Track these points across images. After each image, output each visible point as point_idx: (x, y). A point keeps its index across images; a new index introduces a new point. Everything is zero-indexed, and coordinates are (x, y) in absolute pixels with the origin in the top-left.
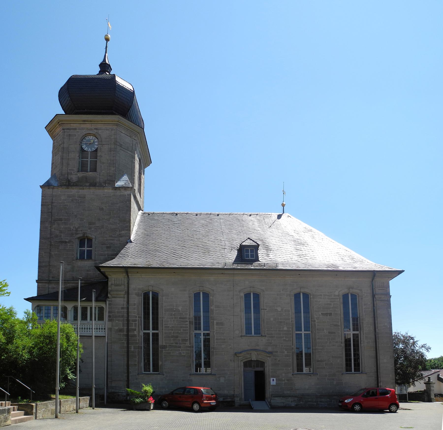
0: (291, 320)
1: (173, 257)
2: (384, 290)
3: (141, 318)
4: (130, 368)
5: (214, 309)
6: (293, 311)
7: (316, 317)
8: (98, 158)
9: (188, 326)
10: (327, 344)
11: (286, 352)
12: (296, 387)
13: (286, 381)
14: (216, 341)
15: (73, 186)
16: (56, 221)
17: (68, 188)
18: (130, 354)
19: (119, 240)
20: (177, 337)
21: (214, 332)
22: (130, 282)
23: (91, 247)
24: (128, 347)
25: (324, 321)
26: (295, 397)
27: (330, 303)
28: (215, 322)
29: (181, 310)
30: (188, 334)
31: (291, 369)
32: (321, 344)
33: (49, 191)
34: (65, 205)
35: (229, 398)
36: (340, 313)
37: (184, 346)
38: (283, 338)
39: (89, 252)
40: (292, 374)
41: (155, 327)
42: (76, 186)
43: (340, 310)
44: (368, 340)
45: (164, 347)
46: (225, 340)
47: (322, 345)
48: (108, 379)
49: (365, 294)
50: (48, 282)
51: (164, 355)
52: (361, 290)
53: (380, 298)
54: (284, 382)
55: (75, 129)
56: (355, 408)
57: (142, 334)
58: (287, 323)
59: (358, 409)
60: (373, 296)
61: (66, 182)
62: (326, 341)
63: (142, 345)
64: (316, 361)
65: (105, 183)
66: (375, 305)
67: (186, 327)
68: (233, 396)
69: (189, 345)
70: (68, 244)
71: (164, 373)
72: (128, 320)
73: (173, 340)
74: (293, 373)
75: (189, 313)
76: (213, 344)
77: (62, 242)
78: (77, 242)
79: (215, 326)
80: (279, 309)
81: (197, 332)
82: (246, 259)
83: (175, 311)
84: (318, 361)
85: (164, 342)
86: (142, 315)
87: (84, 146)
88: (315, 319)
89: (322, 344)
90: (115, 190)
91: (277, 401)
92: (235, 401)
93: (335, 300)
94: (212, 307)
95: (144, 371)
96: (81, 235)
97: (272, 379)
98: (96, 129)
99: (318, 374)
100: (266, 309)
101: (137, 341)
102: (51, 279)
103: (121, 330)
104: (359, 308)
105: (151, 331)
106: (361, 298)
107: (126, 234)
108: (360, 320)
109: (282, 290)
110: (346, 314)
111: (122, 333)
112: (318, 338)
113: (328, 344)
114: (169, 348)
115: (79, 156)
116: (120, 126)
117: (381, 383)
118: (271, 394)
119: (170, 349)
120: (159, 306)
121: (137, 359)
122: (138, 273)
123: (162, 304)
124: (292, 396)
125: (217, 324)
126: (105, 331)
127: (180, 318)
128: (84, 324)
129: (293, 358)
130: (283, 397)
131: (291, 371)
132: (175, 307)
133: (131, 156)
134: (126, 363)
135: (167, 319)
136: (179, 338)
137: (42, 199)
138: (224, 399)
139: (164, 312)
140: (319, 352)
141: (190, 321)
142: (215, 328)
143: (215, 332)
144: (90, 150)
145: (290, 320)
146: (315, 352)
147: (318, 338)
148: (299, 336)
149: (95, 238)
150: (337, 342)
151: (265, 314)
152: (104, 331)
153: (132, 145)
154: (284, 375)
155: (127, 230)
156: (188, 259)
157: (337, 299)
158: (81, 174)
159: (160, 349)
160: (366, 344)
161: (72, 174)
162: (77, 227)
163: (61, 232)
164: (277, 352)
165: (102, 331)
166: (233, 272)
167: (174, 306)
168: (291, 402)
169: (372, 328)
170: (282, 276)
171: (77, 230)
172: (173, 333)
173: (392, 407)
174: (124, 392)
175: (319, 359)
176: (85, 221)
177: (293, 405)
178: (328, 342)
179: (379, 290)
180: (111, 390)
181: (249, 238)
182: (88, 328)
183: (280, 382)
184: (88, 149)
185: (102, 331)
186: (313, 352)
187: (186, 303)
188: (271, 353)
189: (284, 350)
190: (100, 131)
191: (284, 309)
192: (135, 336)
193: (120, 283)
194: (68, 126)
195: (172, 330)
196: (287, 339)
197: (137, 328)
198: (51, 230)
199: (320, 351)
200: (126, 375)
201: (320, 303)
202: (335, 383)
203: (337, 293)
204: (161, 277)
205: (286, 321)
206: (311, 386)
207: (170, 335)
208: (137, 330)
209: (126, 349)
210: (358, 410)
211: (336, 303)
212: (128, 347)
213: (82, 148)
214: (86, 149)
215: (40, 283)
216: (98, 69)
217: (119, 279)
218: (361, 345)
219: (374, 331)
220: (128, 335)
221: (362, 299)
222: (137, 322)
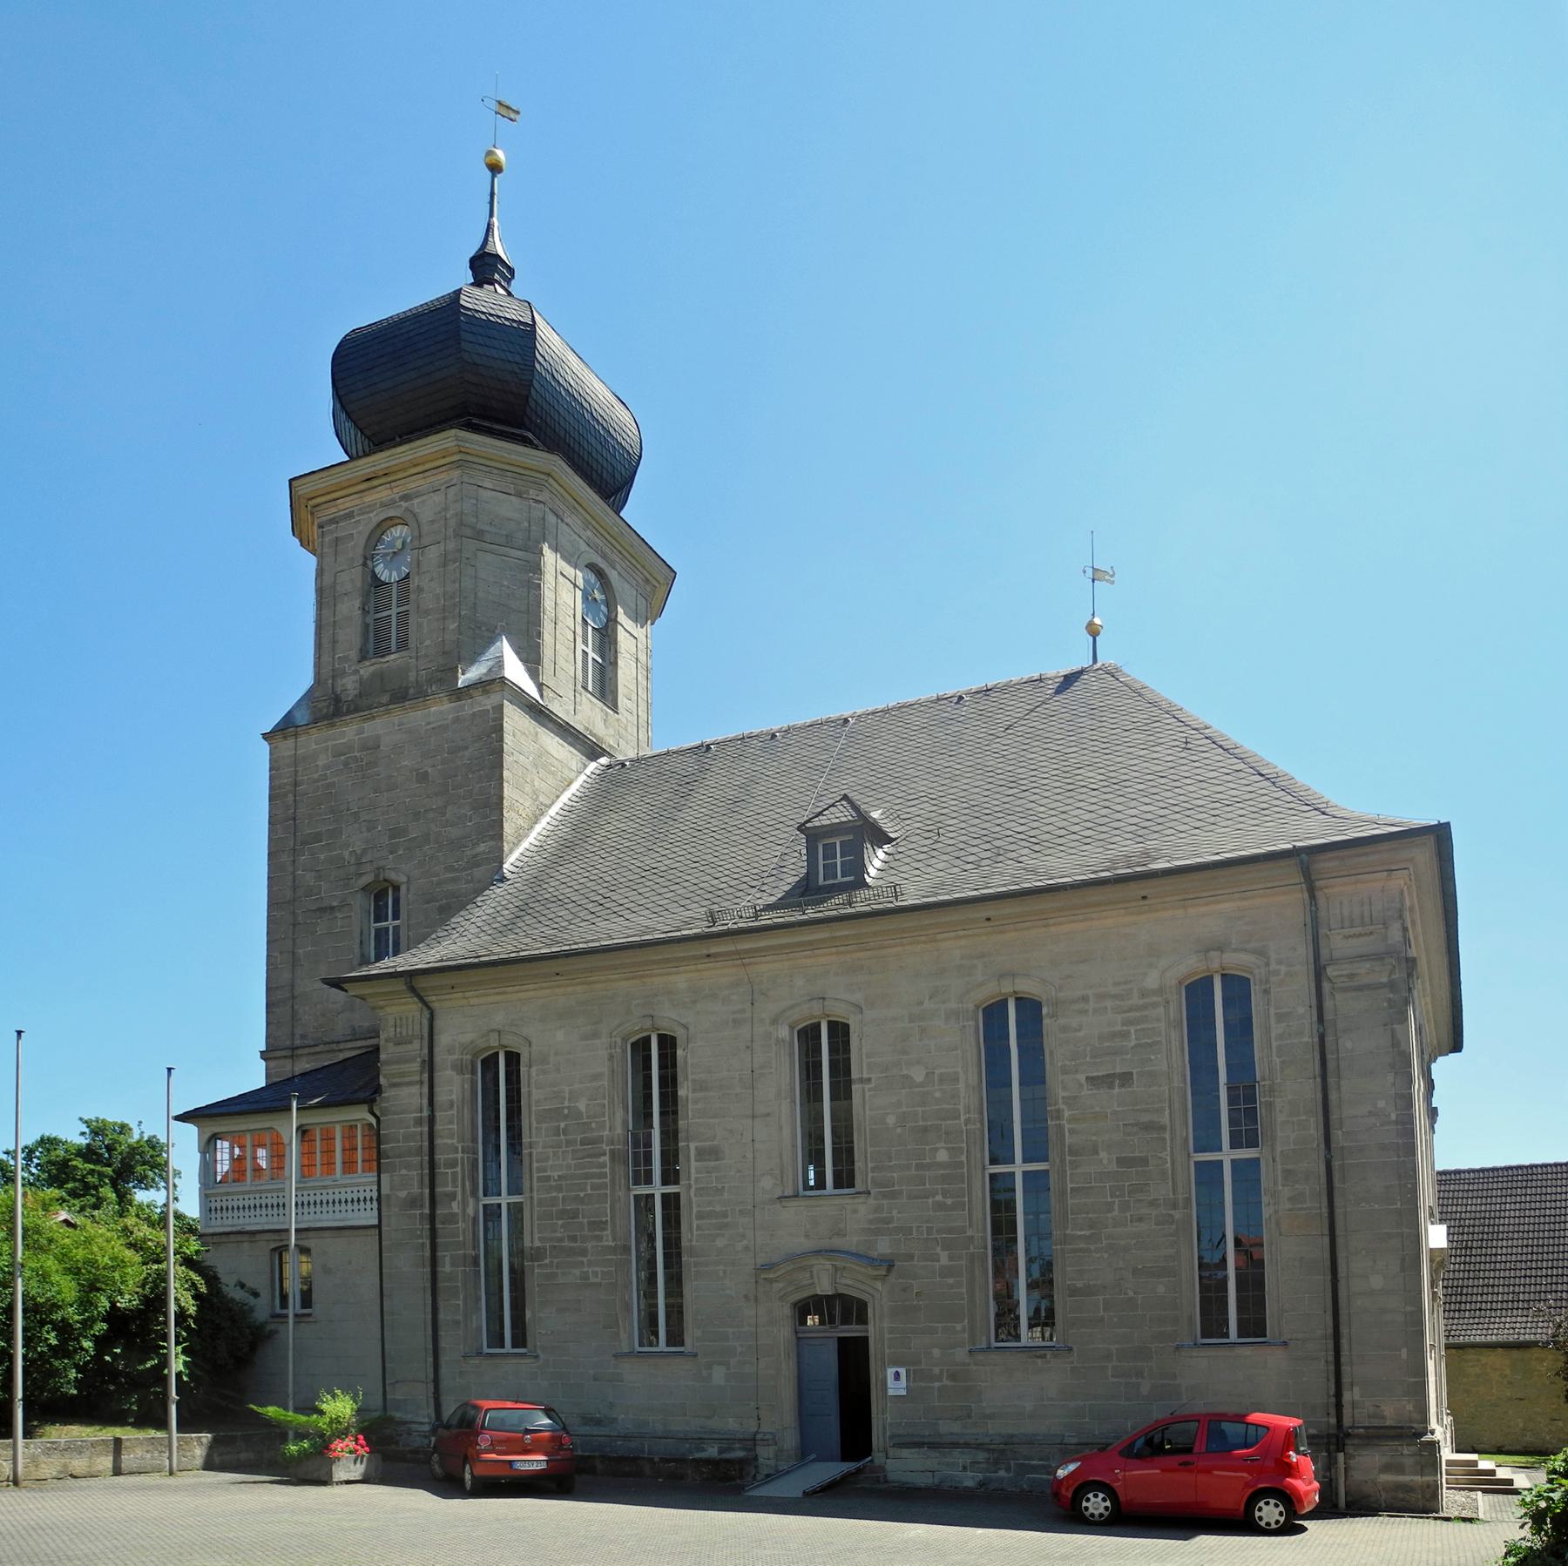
2: (1371, 933)
5: (690, 1095)
7: (1063, 1098)
9: (608, 1170)
10: (1110, 1215)
12: (984, 1404)
13: (946, 1382)
15: (349, 712)
17: (333, 725)
18: (441, 1285)
20: (575, 1214)
21: (690, 1186)
22: (438, 1024)
25: (1098, 1109)
26: (979, 1447)
27: (1125, 1028)
29: (584, 1111)
31: (964, 1330)
32: (1088, 1213)
35: (737, 1445)
38: (934, 1197)
42: (357, 710)
43: (1173, 1056)
44: (1297, 1186)
46: (725, 1215)
47: (1091, 1219)
49: (1283, 969)
50: (288, 1053)
51: (539, 1285)
52: (1261, 953)
53: (1351, 976)
54: (937, 1384)
55: (350, 515)
56: (1086, 1508)
58: (947, 1133)
59: (1102, 1510)
60: (1319, 974)
61: (328, 707)
62: (1109, 1200)
65: (430, 682)
66: (1328, 1016)
68: (752, 1441)
71: (539, 1352)
72: (432, 1164)
73: (562, 1226)
74: (974, 1344)
77: (322, 910)
78: (361, 904)
80: (918, 1075)
82: (826, 883)
83: (566, 1117)
84: (1074, 1292)
85: (536, 1236)
89: (1090, 1216)
90: (459, 699)
91: (904, 1466)
92: (761, 1460)
93: (1146, 1013)
96: (367, 879)
97: (894, 1370)
98: (406, 498)
99: (1075, 1349)
100: (869, 1080)
101: (461, 1239)
102: (298, 1042)
105: (657, 1190)
106: (1264, 987)
109: (931, 998)
112: (1072, 1189)
113: (1116, 1213)
116: (474, 466)
118: (888, 1433)
119: (555, 1261)
121: (461, 1303)
122: (455, 990)
124: (967, 1445)
127: (582, 1144)
130: (933, 1446)
131: (966, 1335)
132: (566, 1104)
133: (525, 563)
136: (580, 1220)
137: (271, 778)
138: (721, 1451)
140: (1076, 1251)
141: (613, 1152)
142: (693, 1171)
145: (959, 1118)
147: (1072, 1189)
149: (408, 882)
150: (1153, 1203)
151: (868, 1103)
153: (526, 524)
154: (936, 1352)
155: (492, 838)
157: (1155, 1005)
158: (367, 670)
160: (1288, 1206)
164: (911, 1257)
166: (731, 948)
167: (564, 1098)
168: (964, 1472)
169: (1314, 1130)
170: (923, 938)
172: (564, 1199)
173: (1260, 1509)
175: (1079, 1284)
177: (969, 1483)
178: (1116, 1207)
179: (1350, 936)
181: (845, 797)
183: (924, 1385)
187: (600, 1083)
188: (889, 1264)
189: (938, 1250)
190: (416, 501)
191: (937, 1072)
192: (452, 1218)
193: (410, 1033)
194: (331, 512)
195: (559, 1189)
197: (459, 1190)
198: (293, 873)
201: (1081, 1034)
202: (1145, 1389)
203: (1152, 981)
204: (522, 995)
205: (943, 1123)
206: (1045, 1403)
207: (554, 1209)
208: (459, 1197)
210: (1101, 1515)
211: (1150, 1026)
213: (374, 575)
215: (270, 1059)
217: (407, 1018)
219: (1322, 1140)
220: (432, 1217)
221: (1267, 992)
222: (459, 1169)
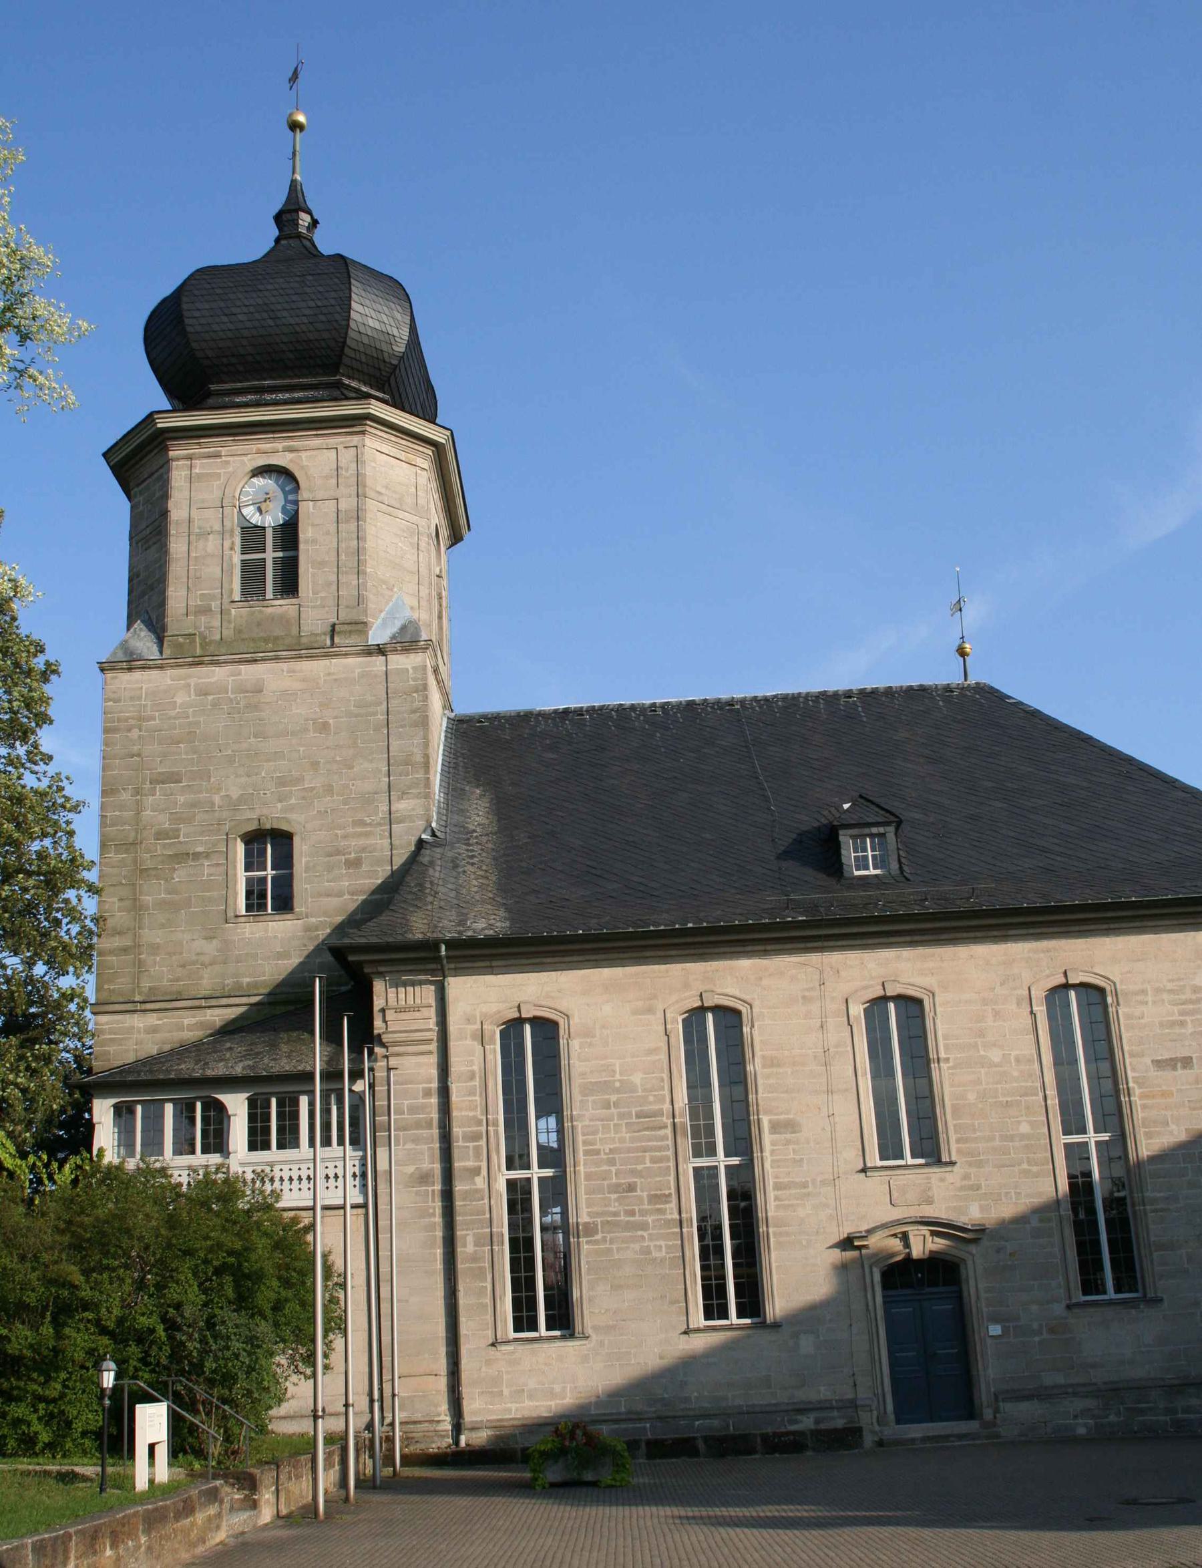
13: (1045, 1336)
30: (670, 1175)
34: (190, 723)
37: (657, 1220)
46: (804, 1185)
54: (1037, 1339)
64: (1153, 1249)
67: (660, 1149)
73: (617, 1200)
74: (1070, 1298)
79: (767, 1138)
83: (617, 1091)
103: (424, 1178)
109: (1001, 985)
114: (603, 1232)
118: (992, 1390)
119: (609, 1236)
127: (638, 1116)
131: (1062, 1291)
132: (618, 1077)
135: (592, 1123)
138: (817, 1422)
143: (769, 1160)
146: (1145, 1210)
152: (308, 1186)
154: (1034, 1308)
165: (300, 1189)
176: (263, 774)
177: (1082, 1431)
185: (300, 1189)
190: (303, 455)
195: (612, 1162)
197: (484, 1165)
201: (1142, 1021)
207: (606, 1183)
208: (484, 1172)
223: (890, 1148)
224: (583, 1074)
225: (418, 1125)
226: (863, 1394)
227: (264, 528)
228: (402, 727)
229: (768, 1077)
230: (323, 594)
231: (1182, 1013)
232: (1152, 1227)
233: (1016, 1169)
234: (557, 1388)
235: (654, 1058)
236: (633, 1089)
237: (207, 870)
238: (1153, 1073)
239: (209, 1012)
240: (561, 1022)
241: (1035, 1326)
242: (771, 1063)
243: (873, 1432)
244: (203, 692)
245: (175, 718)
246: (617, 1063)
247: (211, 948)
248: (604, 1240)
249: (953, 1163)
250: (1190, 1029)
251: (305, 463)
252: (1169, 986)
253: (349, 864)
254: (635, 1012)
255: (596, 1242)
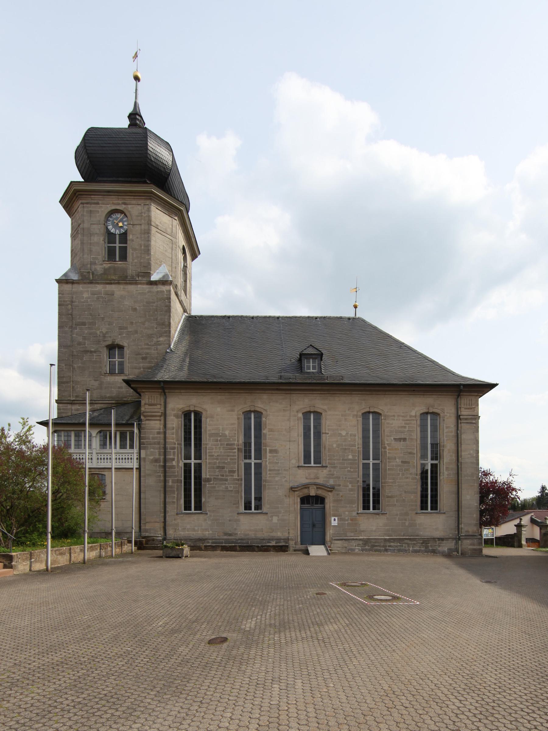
0: (357, 447)
1: (221, 370)
3: (181, 444)
4: (167, 506)
6: (361, 435)
8: (128, 242)
11: (350, 486)
13: (349, 522)
14: (268, 472)
16: (78, 325)
18: (167, 489)
19: (157, 349)
20: (223, 468)
21: (266, 461)
23: (123, 359)
24: (165, 481)
28: (268, 449)
33: (67, 287)
34: (89, 305)
35: (282, 541)
36: (415, 437)
39: (121, 364)
40: (356, 512)
41: (198, 456)
45: (208, 480)
46: (279, 470)
48: (142, 521)
49: (448, 415)
54: (347, 522)
57: (181, 464)
63: (181, 477)
66: (459, 429)
67: (233, 456)
69: (237, 477)
70: (95, 355)
71: (208, 512)
72: (165, 448)
73: (218, 471)
75: (238, 438)
76: (266, 475)
77: (86, 352)
79: (268, 454)
81: (247, 461)
83: (220, 436)
84: (388, 497)
85: (208, 474)
86: (182, 442)
87: (110, 227)
88: (386, 445)
94: (264, 431)
95: (185, 510)
101: (176, 474)
103: (156, 461)
104: (440, 432)
105: (193, 461)
107: (164, 341)
108: (440, 447)
109: (348, 410)
110: (424, 438)
111: (158, 464)
115: (104, 240)
117: (462, 524)
119: (215, 482)
120: (203, 430)
123: (206, 427)
125: (271, 451)
126: (111, 461)
128: (80, 453)
129: (358, 494)
134: (162, 500)
137: (59, 298)
139: (208, 438)
141: (238, 449)
144: (117, 232)
148: (366, 467)
150: (411, 474)
154: (347, 513)
156: (238, 372)
157: (413, 420)
158: (107, 265)
159: (203, 483)
161: (96, 264)
162: (104, 332)
163: (84, 338)
164: (339, 485)
171: (104, 336)
172: (219, 463)
174: (160, 535)
175: (390, 495)
180: (144, 534)
181: (311, 345)
182: (106, 458)
184: (115, 231)
186: (382, 486)
189: (348, 484)
190: (129, 206)
192: (173, 467)
195: (217, 459)
196: (352, 470)
197: (176, 457)
198: (71, 335)
199: (391, 484)
200: (163, 515)
201: (392, 425)
207: (215, 466)
208: (176, 459)
209: (162, 484)
212: (165, 481)
214: (113, 231)
216: (128, 122)
218: (440, 478)
220: (165, 467)
221: (444, 420)
222: (176, 450)
223: (307, 459)
224: (210, 430)
225: (155, 443)
226: (291, 536)
227: (115, 234)
228: (161, 311)
229: (270, 435)
230: (135, 261)
231: (405, 424)
232: (386, 490)
233: (346, 469)
234: (196, 528)
235: (233, 426)
236: (226, 436)
237: (95, 357)
238: (393, 442)
239: (96, 405)
240: (203, 412)
241: (347, 518)
242: (271, 430)
243: (293, 547)
244: (93, 294)
245: (84, 302)
246: (221, 427)
247: (96, 384)
248: (213, 483)
249: (327, 467)
250: (407, 429)
251: (130, 210)
252: (402, 414)
253: (143, 358)
254: (229, 411)
255: (211, 484)
